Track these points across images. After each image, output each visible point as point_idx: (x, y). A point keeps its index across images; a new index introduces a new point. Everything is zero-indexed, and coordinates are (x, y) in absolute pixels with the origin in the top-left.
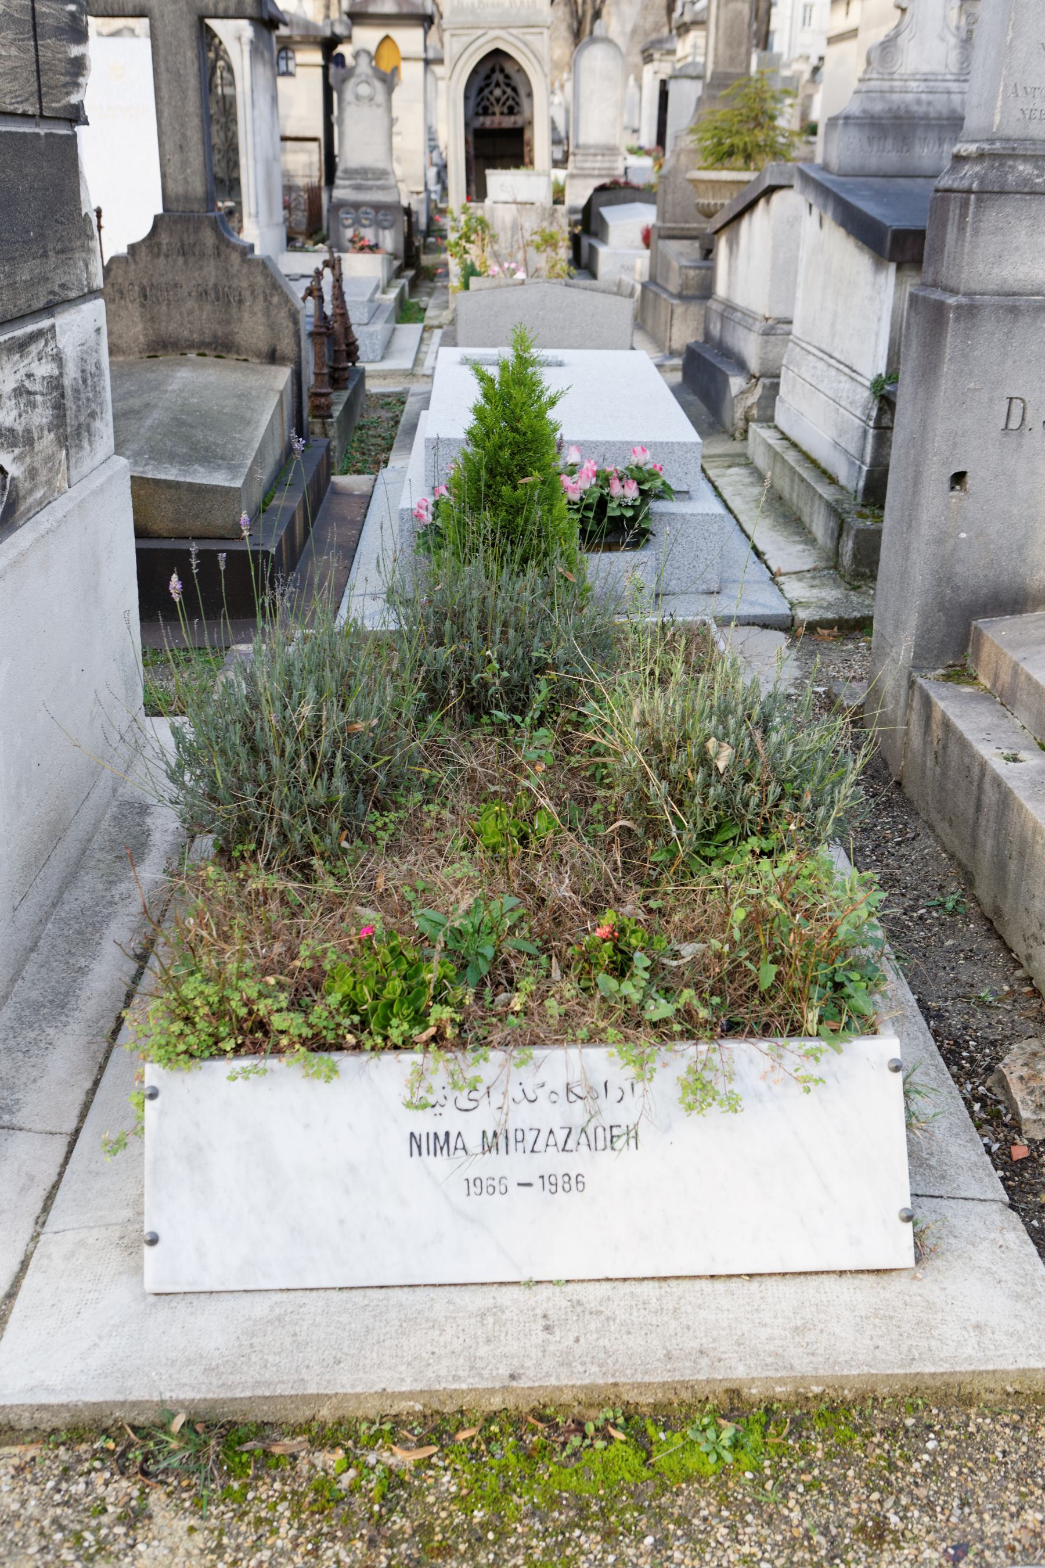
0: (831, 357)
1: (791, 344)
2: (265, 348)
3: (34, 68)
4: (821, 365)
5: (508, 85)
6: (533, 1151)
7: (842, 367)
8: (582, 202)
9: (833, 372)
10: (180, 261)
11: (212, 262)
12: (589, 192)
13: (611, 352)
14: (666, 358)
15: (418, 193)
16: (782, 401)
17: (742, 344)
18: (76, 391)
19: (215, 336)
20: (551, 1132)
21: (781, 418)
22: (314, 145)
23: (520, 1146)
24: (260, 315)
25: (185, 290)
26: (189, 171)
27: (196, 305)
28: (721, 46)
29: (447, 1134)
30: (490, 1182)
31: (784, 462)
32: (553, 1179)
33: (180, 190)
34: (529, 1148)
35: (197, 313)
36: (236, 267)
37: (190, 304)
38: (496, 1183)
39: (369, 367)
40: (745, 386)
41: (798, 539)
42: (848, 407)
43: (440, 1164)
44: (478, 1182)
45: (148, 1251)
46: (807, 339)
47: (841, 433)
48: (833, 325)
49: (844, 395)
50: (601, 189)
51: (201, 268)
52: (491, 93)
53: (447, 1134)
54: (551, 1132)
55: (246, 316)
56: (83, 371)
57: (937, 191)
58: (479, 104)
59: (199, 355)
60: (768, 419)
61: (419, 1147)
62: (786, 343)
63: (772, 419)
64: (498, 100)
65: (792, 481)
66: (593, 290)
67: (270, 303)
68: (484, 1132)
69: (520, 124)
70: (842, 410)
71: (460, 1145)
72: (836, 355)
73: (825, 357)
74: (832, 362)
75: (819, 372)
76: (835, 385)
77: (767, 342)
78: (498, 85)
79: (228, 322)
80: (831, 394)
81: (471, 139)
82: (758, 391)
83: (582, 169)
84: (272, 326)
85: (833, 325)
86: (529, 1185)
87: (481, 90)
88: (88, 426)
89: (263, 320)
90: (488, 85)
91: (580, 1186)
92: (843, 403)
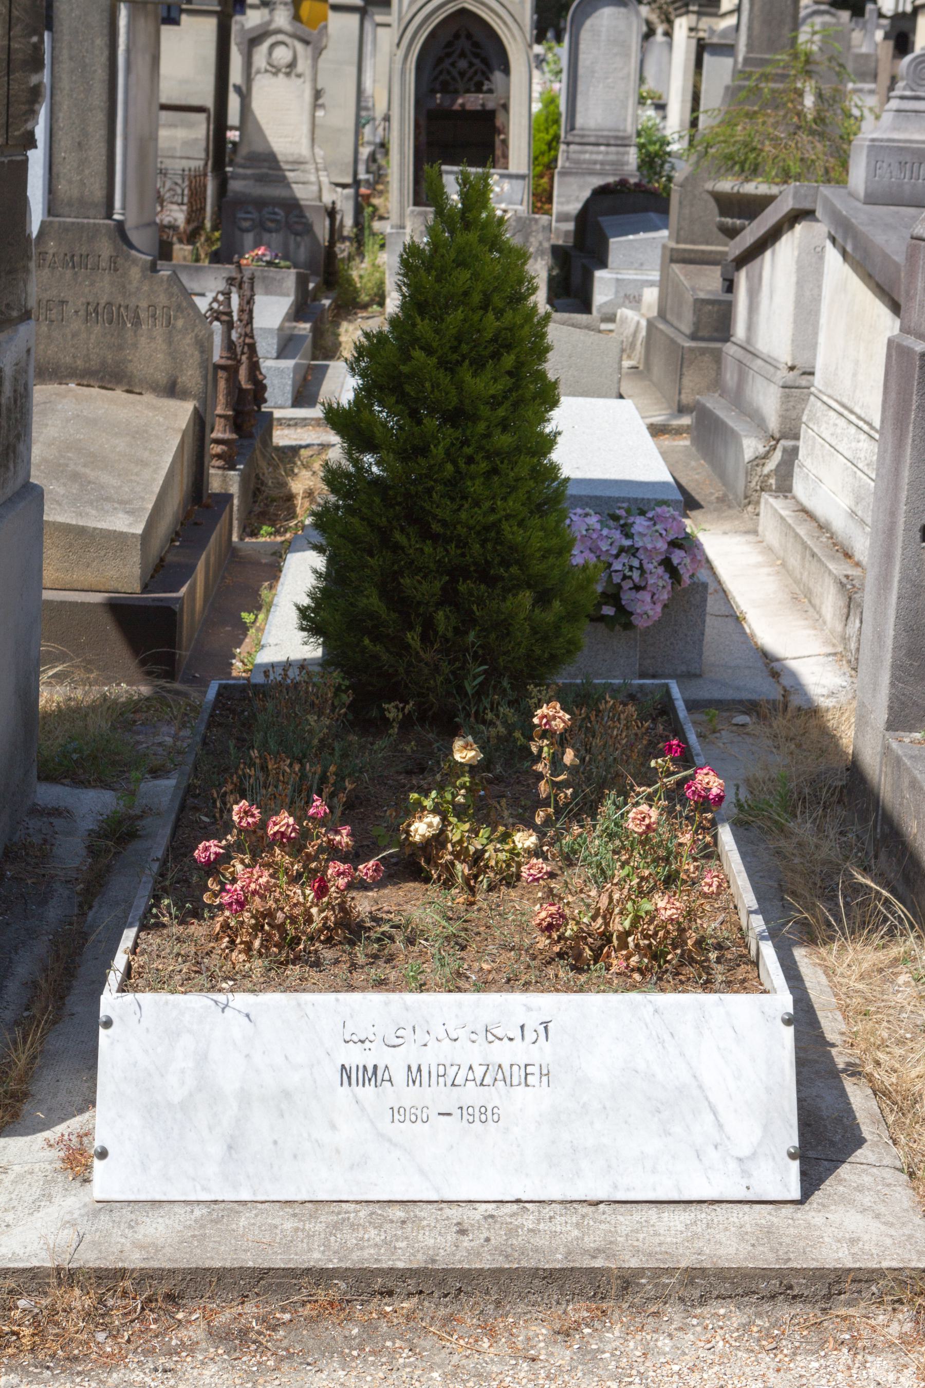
0: (852, 412)
1: (812, 398)
2: (162, 378)
3: (5, 102)
4: (842, 422)
5: (477, 55)
6: (453, 1085)
7: (861, 424)
8: (574, 207)
9: (853, 430)
10: (69, 273)
11: (107, 278)
12: (587, 194)
13: (589, 400)
14: (673, 416)
15: (344, 186)
16: (802, 466)
17: (761, 398)
18: (9, 410)
19: (103, 363)
20: (471, 1068)
21: (799, 488)
22: (202, 117)
23: (441, 1079)
24: (160, 340)
25: (70, 310)
26: (87, 172)
27: (83, 327)
28: (757, 25)
29: (375, 1067)
30: (413, 1110)
31: (797, 535)
32: (470, 1110)
33: (75, 193)
34: (449, 1083)
35: (84, 336)
36: (135, 284)
37: (76, 324)
38: (419, 1113)
39: (277, 414)
40: (762, 450)
41: (803, 623)
42: (865, 469)
43: (368, 1092)
44: (402, 1110)
45: (97, 1163)
46: (830, 392)
47: (858, 500)
48: (855, 375)
49: (862, 456)
50: (600, 192)
51: (92, 284)
52: (453, 64)
53: (375, 1067)
54: (471, 1068)
55: (143, 340)
56: (15, 391)
57: (912, 238)
58: (436, 78)
59: (79, 385)
60: (784, 488)
61: (349, 1078)
62: (805, 400)
63: (790, 489)
64: (462, 74)
65: (803, 558)
66: (573, 325)
67: (174, 327)
68: (409, 1068)
69: (490, 105)
70: (859, 473)
71: (386, 1077)
72: (857, 410)
73: (846, 413)
74: (852, 418)
75: (839, 431)
76: (854, 445)
77: (788, 396)
78: (463, 55)
79: (121, 348)
80: (848, 454)
81: (423, 122)
82: (777, 456)
83: (578, 162)
84: (174, 355)
85: (855, 375)
86: (449, 1114)
87: (440, 60)
88: (15, 447)
89: (164, 347)
90: (448, 55)
91: (496, 1117)
92: (860, 465)
